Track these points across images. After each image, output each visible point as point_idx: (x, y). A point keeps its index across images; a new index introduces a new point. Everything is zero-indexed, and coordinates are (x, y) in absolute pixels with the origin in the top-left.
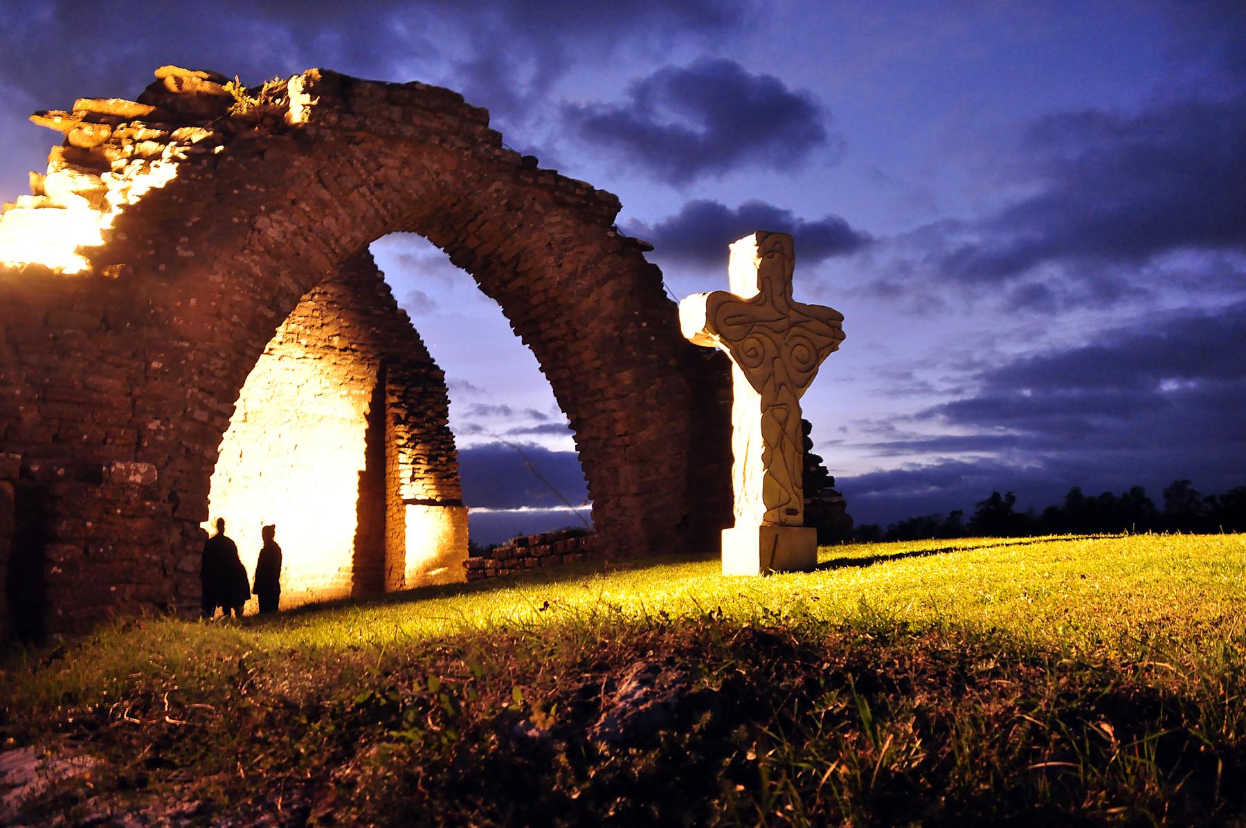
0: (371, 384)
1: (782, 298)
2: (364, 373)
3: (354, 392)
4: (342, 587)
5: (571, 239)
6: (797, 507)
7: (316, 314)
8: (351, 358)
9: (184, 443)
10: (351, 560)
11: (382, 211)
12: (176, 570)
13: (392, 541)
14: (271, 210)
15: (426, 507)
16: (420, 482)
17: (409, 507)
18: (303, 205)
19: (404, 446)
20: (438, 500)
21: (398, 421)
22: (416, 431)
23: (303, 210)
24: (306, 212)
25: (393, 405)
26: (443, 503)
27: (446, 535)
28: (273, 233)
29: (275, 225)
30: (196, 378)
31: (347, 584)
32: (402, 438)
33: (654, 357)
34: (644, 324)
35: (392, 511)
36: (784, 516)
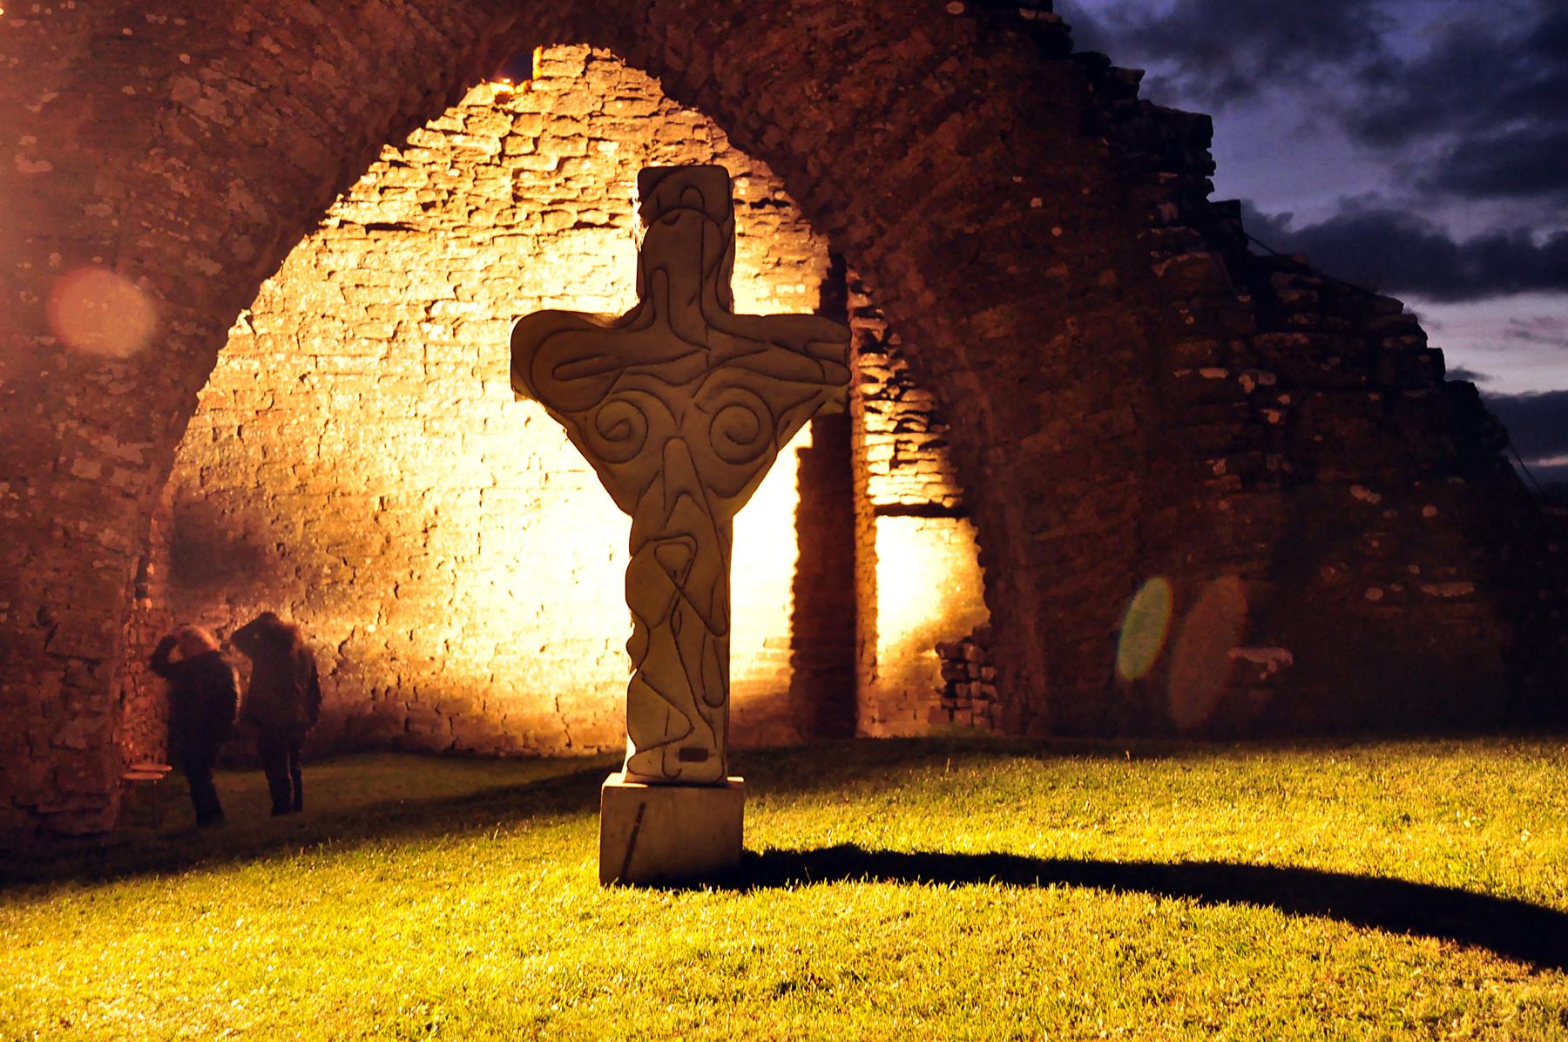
0: (816, 270)
1: (694, 308)
2: (803, 250)
3: (782, 290)
4: (772, 676)
5: (860, 32)
6: (709, 745)
7: (701, 135)
8: (775, 220)
9: (58, 520)
10: (787, 624)
11: (432, 34)
12: (51, 745)
13: (863, 588)
14: (203, 59)
15: (918, 521)
16: (909, 470)
17: (882, 522)
18: (266, 43)
19: (877, 397)
20: (948, 503)
21: (870, 345)
22: (902, 364)
23: (267, 53)
24: (273, 56)
25: (862, 313)
26: (954, 513)
27: (962, 576)
28: (208, 107)
29: (209, 90)
30: (73, 401)
31: (780, 672)
32: (874, 380)
33: (1061, 271)
34: (1036, 202)
35: (862, 523)
36: (675, 765)
